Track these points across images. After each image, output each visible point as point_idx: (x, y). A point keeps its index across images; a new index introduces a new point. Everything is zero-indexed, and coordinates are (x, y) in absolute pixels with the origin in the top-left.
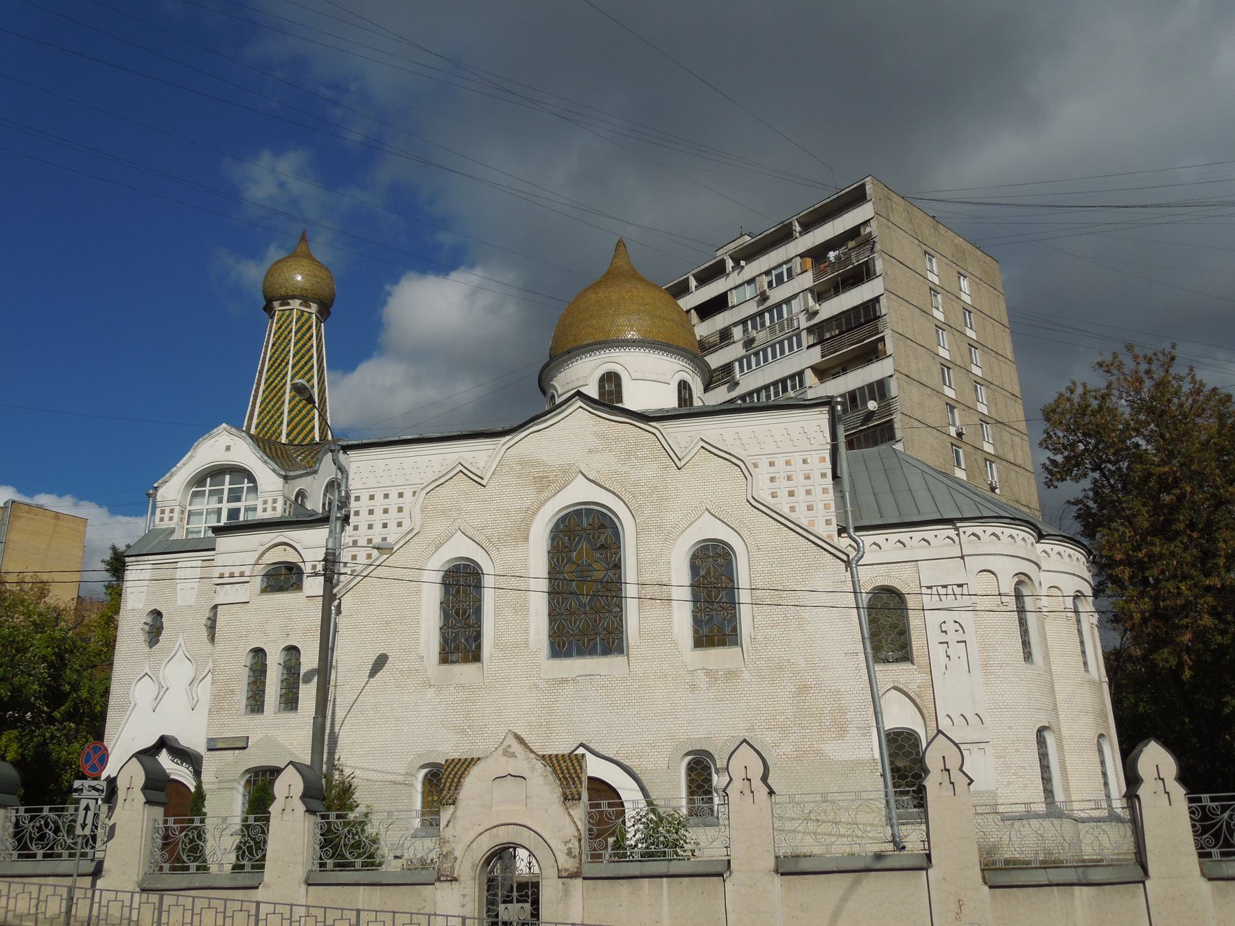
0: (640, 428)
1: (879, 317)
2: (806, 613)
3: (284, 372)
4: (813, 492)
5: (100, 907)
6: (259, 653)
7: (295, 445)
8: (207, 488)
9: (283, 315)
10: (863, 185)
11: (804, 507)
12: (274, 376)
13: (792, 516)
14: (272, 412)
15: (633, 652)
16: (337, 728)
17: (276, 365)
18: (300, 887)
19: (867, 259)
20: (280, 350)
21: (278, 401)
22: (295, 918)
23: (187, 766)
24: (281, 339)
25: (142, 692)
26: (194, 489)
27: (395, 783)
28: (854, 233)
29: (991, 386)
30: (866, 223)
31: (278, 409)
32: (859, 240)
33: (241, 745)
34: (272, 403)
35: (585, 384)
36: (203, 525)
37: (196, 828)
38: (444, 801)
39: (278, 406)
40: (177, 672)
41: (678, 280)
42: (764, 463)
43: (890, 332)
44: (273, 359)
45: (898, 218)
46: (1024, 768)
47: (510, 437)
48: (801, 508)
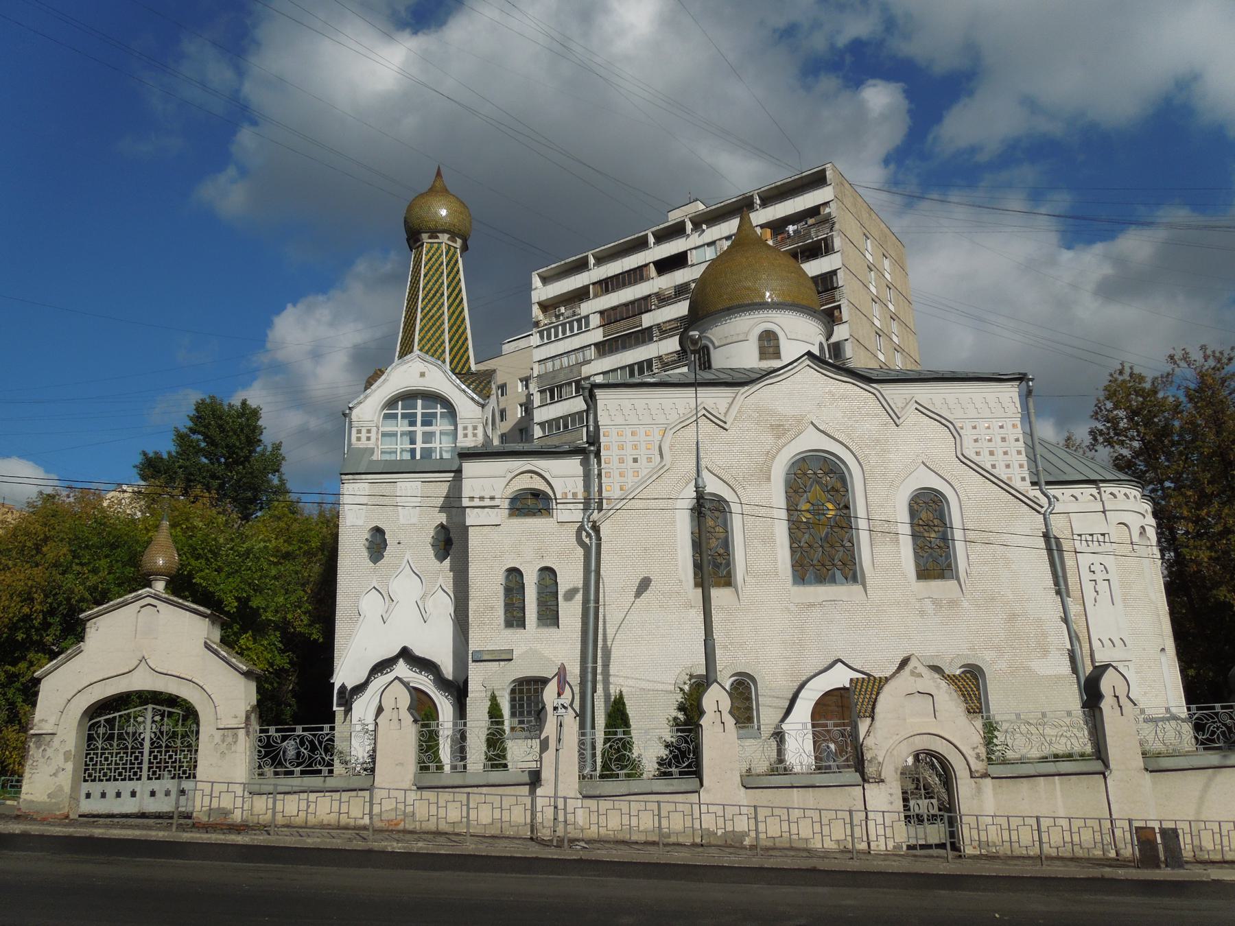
0: (862, 388)
1: (836, 288)
3: (440, 303)
4: (982, 453)
5: (565, 814)
6: (514, 574)
8: (400, 411)
9: (431, 248)
10: (824, 171)
11: (1003, 464)
12: (430, 306)
14: (433, 340)
15: (869, 582)
16: (609, 643)
17: (431, 295)
18: (740, 790)
20: (433, 281)
21: (437, 331)
24: (433, 270)
25: (371, 604)
26: (385, 411)
28: (814, 211)
29: (904, 353)
30: (826, 204)
31: (438, 339)
32: (818, 218)
33: (505, 657)
36: (399, 447)
39: (437, 335)
40: (405, 587)
41: (636, 236)
42: (968, 425)
43: (846, 301)
44: (427, 289)
45: (848, 202)
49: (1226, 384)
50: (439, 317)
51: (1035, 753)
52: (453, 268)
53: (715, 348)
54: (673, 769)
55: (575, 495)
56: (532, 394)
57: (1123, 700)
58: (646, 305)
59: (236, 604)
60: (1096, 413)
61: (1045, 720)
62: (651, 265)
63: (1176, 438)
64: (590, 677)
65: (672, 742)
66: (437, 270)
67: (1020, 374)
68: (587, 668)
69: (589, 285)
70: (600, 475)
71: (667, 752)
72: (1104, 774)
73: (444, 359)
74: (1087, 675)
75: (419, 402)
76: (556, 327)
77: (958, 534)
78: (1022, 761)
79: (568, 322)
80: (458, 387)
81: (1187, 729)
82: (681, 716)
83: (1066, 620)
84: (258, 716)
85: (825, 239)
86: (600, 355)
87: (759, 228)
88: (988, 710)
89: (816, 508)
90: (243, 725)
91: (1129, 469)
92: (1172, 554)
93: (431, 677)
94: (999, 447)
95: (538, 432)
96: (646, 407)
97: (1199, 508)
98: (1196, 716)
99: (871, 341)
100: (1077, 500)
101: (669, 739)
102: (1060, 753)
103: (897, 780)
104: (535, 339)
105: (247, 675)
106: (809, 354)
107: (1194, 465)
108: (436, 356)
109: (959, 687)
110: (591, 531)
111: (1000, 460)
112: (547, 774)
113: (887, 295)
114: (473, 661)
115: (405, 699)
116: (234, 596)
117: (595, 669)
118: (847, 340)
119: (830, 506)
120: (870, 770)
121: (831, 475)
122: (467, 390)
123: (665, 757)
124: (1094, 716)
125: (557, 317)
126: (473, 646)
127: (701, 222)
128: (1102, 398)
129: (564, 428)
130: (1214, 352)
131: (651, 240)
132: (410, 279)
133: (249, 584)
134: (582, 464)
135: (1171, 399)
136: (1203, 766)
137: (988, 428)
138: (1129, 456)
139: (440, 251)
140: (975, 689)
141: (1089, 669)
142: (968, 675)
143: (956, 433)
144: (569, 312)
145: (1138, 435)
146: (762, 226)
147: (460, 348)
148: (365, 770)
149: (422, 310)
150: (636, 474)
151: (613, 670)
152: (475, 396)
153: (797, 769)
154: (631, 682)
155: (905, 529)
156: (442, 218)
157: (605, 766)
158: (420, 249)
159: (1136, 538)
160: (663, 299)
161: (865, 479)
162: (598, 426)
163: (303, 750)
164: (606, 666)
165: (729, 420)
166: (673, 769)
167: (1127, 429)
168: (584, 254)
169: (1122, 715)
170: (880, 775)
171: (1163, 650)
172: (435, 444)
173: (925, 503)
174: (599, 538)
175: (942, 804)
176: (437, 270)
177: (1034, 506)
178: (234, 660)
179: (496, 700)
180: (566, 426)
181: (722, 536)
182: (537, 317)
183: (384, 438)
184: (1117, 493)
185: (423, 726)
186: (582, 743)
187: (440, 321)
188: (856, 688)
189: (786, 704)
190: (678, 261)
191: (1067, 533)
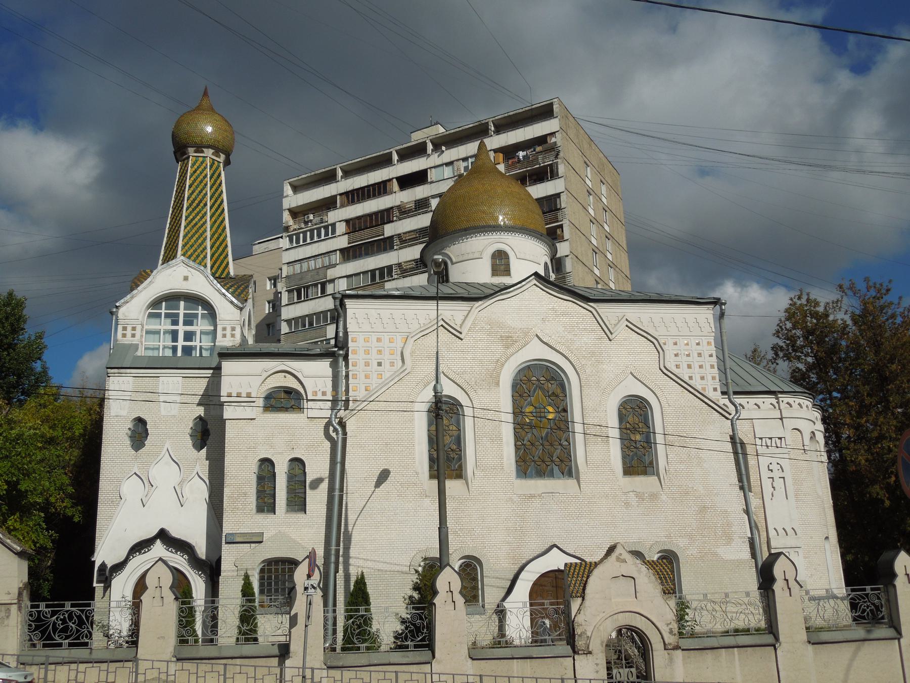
2: (704, 455)
3: (203, 212)
6: (267, 464)
7: (223, 278)
8: (163, 311)
9: (197, 161)
10: (551, 105)
11: (698, 377)
12: (193, 214)
13: (690, 382)
14: (196, 246)
15: (582, 476)
16: (350, 528)
17: (195, 204)
18: (467, 661)
19: (551, 162)
20: (197, 192)
22: (259, 676)
23: (181, 554)
25: (131, 488)
26: (150, 311)
27: (402, 572)
28: (542, 140)
31: (200, 245)
32: (545, 146)
33: (256, 540)
34: (195, 238)
35: (480, 257)
36: (161, 344)
37: (362, 616)
38: (574, 594)
39: (200, 241)
41: (381, 153)
42: (670, 342)
43: (568, 222)
44: (191, 199)
45: (572, 133)
46: (819, 565)
47: (482, 302)
48: (697, 377)
49: (884, 311)
50: (202, 226)
51: (719, 628)
52: (216, 181)
53: (453, 263)
54: (409, 643)
55: (324, 394)
56: (281, 293)
57: (792, 583)
58: (388, 216)
59: (6, 487)
60: (778, 332)
61: (728, 600)
62: (395, 180)
63: (843, 356)
64: (333, 559)
65: (408, 618)
66: (201, 182)
67: (714, 298)
68: (330, 550)
69: (335, 196)
70: (347, 376)
71: (403, 627)
72: (774, 646)
73: (206, 264)
74: (764, 559)
75: (182, 303)
76: (305, 233)
77: (659, 439)
78: (709, 635)
79: (316, 229)
80: (218, 291)
81: (844, 608)
82: (416, 595)
83: (747, 512)
84: (29, 592)
85: (551, 165)
86: (344, 261)
87: (492, 152)
88: (681, 591)
89: (538, 410)
90: (16, 601)
91: (804, 381)
92: (837, 455)
93: (186, 557)
94: (696, 361)
95: (285, 329)
96: (391, 317)
97: (859, 416)
98: (850, 596)
99: (588, 258)
100: (759, 407)
101: (405, 616)
102: (741, 628)
103: (602, 652)
104: (284, 243)
105: (21, 554)
106: (536, 274)
107: (857, 379)
108: (198, 261)
109: (657, 571)
110: (338, 427)
111: (696, 373)
112: (296, 647)
113: (602, 216)
114: (226, 543)
115: (168, 579)
116: (4, 480)
117: (338, 551)
118: (567, 256)
119: (551, 409)
120: (580, 643)
121: (552, 382)
122: (227, 294)
123: (400, 632)
124: (768, 597)
125: (306, 223)
126: (227, 528)
127: (440, 144)
128: (783, 319)
129: (309, 325)
130: (875, 284)
131: (395, 157)
132: (175, 189)
133: (19, 469)
134: (331, 366)
135: (840, 322)
136: (854, 639)
137: (687, 344)
138: (804, 369)
139: (204, 165)
140: (670, 573)
141: (766, 555)
142: (665, 561)
143: (659, 348)
144: (317, 219)
145: (811, 352)
146: (495, 151)
147: (220, 255)
148: (127, 642)
149: (187, 218)
150: (380, 376)
151: (352, 552)
152: (234, 300)
153: (517, 642)
154: (370, 564)
155: (615, 433)
156: (207, 134)
157: (347, 639)
158: (186, 161)
159: (807, 441)
160: (404, 212)
161: (581, 386)
162: (347, 332)
163: (71, 624)
164: (347, 548)
165: (464, 330)
166: (409, 643)
167: (803, 346)
168: (335, 167)
169: (791, 595)
170: (588, 648)
171: (827, 538)
172: (196, 343)
173: (631, 408)
174: (345, 433)
175: (640, 672)
176: (201, 182)
177: (723, 413)
178: (8, 541)
179: (249, 579)
180: (311, 324)
181: (455, 433)
182: (287, 222)
183: (148, 335)
184: (792, 403)
185: (183, 603)
186: (326, 619)
187: (202, 229)
188: (569, 572)
189: (508, 584)
190: (419, 178)
191: (751, 436)
